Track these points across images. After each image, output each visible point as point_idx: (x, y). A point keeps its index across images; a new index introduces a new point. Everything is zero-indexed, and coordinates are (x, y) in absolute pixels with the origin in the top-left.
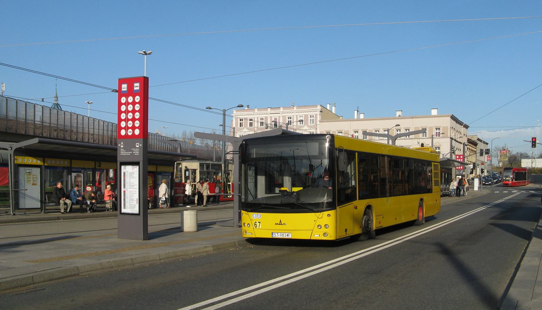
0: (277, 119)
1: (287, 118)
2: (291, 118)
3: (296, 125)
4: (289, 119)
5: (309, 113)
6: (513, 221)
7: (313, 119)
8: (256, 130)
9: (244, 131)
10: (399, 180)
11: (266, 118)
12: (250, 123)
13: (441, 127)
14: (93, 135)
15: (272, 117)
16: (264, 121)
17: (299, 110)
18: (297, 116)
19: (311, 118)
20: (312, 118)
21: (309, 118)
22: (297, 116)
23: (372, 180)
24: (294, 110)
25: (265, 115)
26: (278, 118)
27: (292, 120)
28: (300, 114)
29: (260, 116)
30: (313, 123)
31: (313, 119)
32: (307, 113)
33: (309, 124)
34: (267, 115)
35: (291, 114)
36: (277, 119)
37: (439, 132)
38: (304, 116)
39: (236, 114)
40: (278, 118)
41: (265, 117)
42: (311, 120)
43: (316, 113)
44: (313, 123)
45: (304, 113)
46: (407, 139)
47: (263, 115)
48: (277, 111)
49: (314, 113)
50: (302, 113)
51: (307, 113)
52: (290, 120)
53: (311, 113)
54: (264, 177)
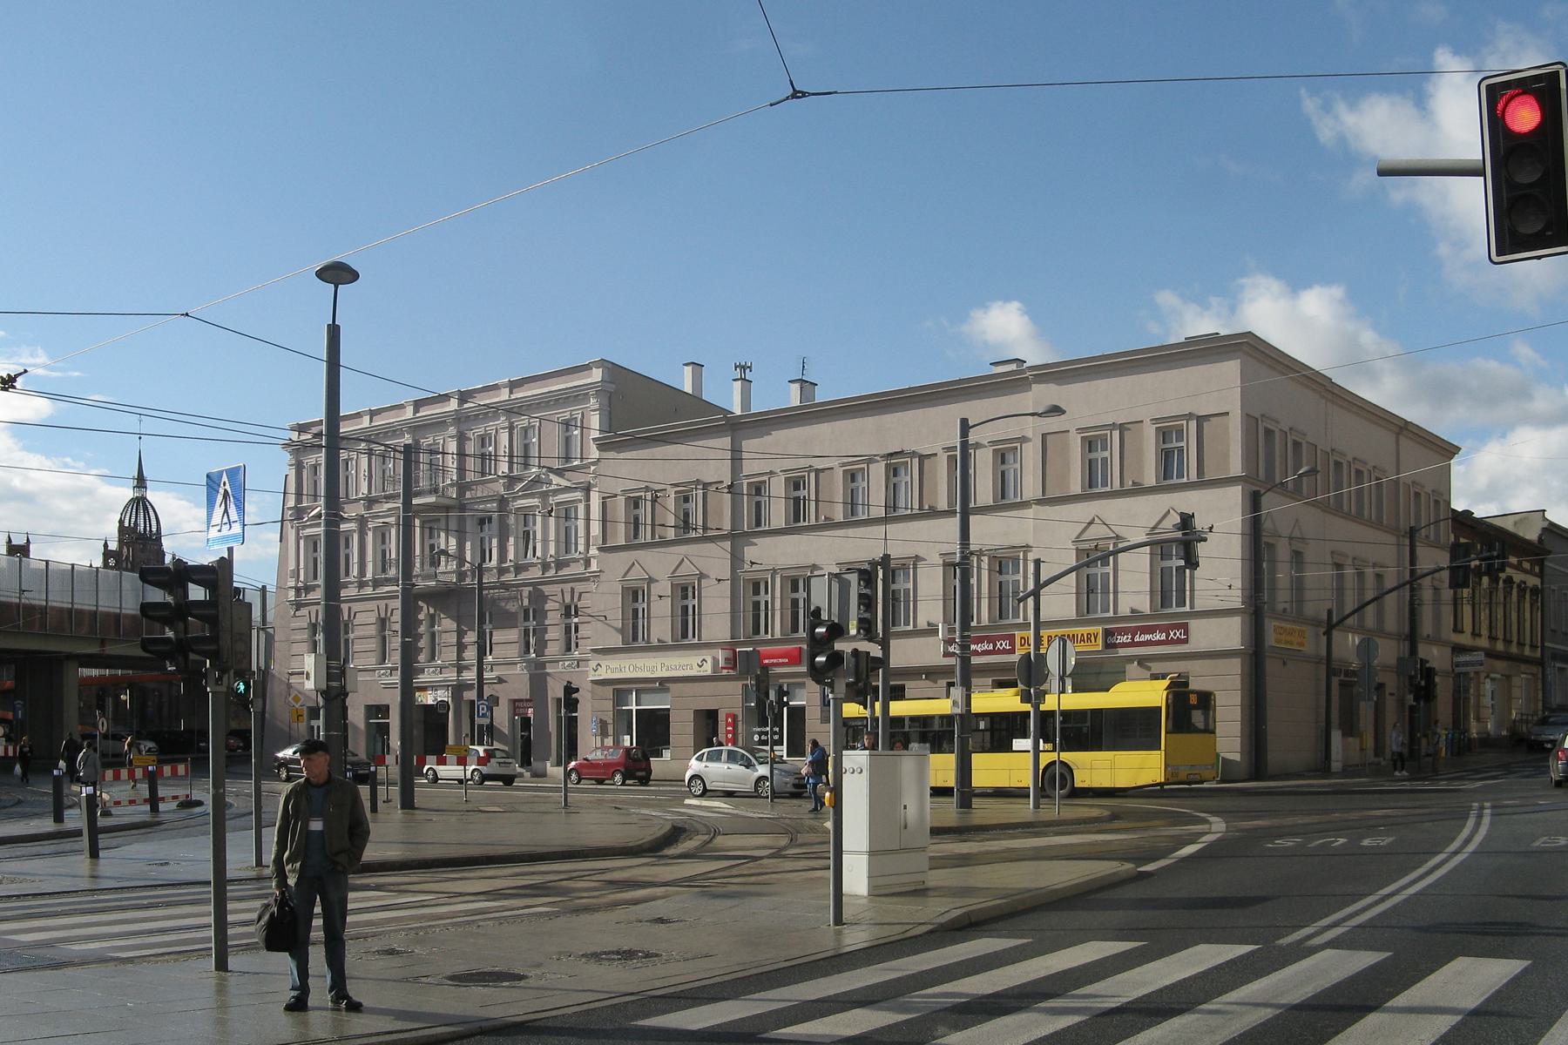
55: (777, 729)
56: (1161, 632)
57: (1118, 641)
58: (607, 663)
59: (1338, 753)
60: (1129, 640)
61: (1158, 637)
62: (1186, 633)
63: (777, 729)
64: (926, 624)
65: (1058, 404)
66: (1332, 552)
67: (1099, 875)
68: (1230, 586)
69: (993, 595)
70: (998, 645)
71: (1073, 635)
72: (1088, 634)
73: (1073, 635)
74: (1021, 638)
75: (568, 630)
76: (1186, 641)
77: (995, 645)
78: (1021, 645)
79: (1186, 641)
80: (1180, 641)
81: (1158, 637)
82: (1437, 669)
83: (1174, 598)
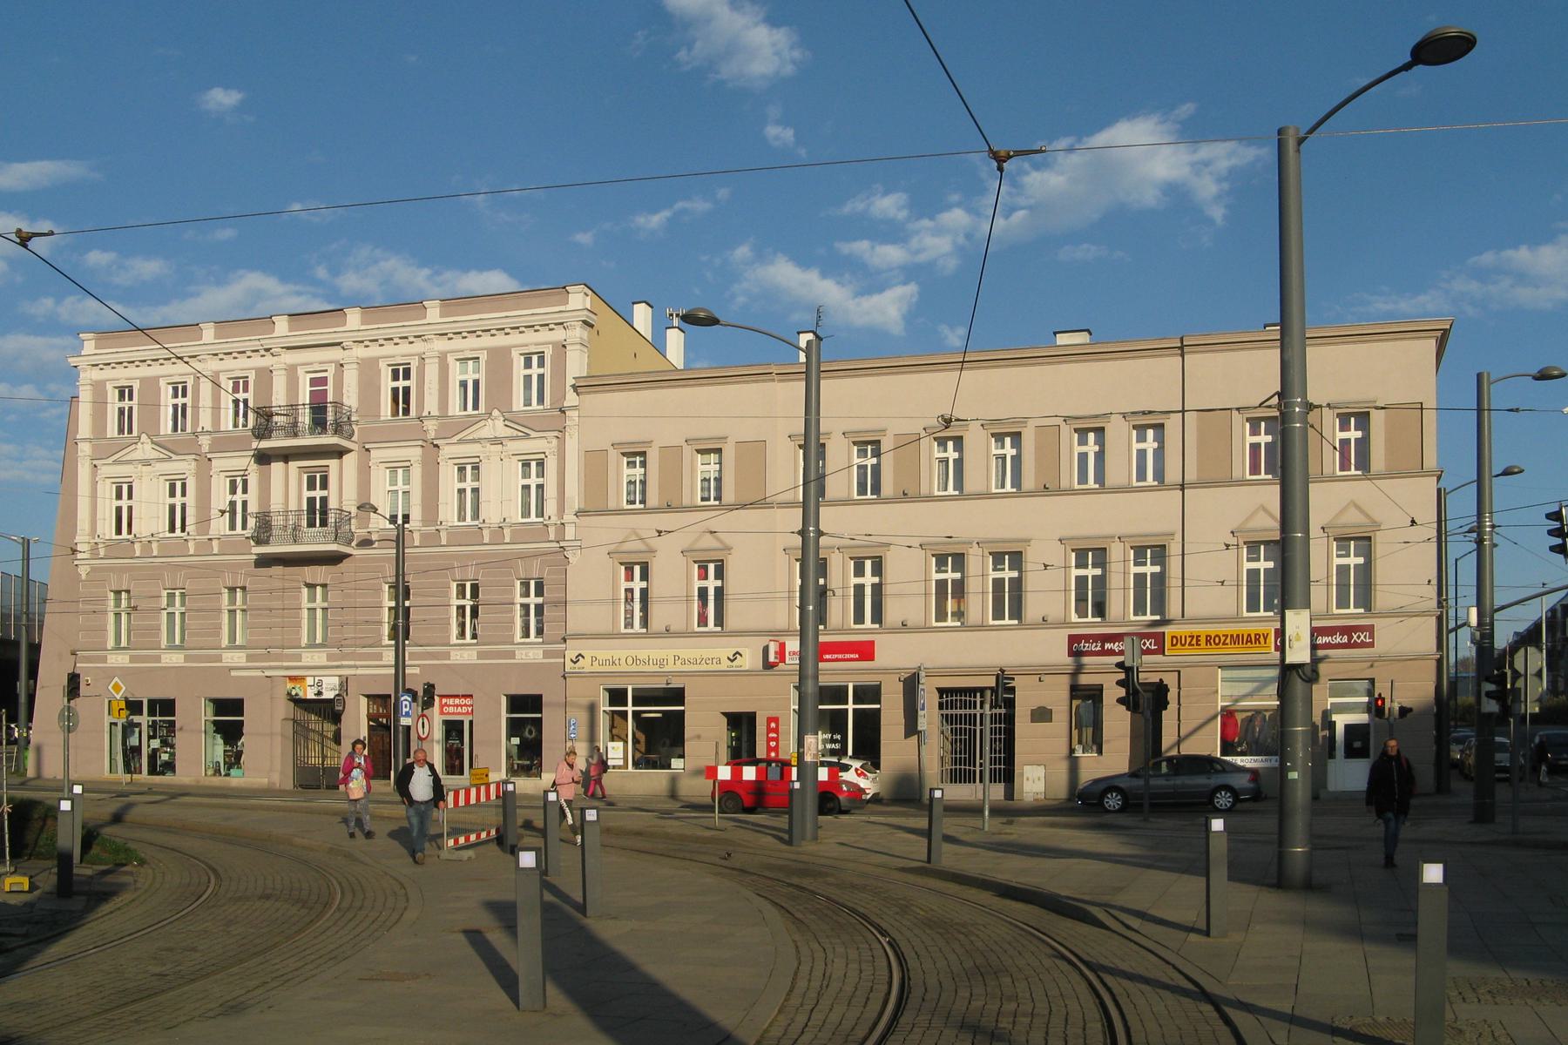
0: (324, 381)
1: (386, 374)
2: (407, 375)
3: (435, 412)
4: (395, 377)
5: (515, 338)
6: (537, 938)
7: (541, 377)
8: (206, 448)
9: (138, 455)
10: (1494, 735)
11: (265, 375)
12: (395, 391)
13: (1024, 420)
14: (338, 405)
15: (300, 371)
16: (250, 396)
17: (376, 326)
18: (442, 358)
19: (528, 372)
20: (535, 371)
21: (519, 371)
22: (442, 358)
23: (528, 762)
24: (569, 307)
25: (258, 362)
26: (330, 375)
27: (412, 383)
28: (458, 343)
29: (229, 363)
30: (541, 400)
31: (541, 377)
32: (500, 340)
33: (518, 404)
34: (267, 361)
35: (404, 348)
36: (324, 381)
37: (321, 498)
38: (483, 357)
39: (95, 359)
40: (330, 375)
41: (143, 380)
42: (528, 379)
43: (559, 335)
44: (541, 400)
45: (487, 341)
46: (868, 502)
47: (242, 362)
48: (411, 326)
49: (544, 335)
50: (472, 342)
51: (500, 340)
52: (401, 384)
53: (530, 337)
54: (754, 778)
55: (839, 737)
56: (1342, 634)
57: (1086, 649)
58: (594, 653)
59: (1255, 761)
60: (1099, 648)
61: (1338, 639)
62: (1372, 636)
63: (839, 737)
64: (1041, 619)
65: (1477, 45)
66: (789, 437)
67: (1097, 832)
68: (1223, 582)
69: (102, 521)
70: (1355, 637)
71: (1238, 636)
72: (1256, 635)
73: (1238, 636)
74: (1173, 637)
75: (629, 595)
76: (1371, 645)
77: (1350, 638)
78: (1172, 645)
79: (1371, 645)
80: (1363, 645)
81: (1338, 639)
82: (704, 777)
83: (1007, 590)
